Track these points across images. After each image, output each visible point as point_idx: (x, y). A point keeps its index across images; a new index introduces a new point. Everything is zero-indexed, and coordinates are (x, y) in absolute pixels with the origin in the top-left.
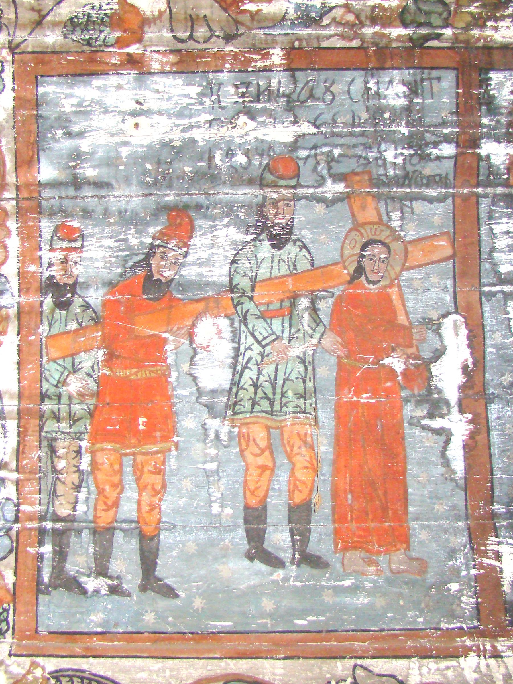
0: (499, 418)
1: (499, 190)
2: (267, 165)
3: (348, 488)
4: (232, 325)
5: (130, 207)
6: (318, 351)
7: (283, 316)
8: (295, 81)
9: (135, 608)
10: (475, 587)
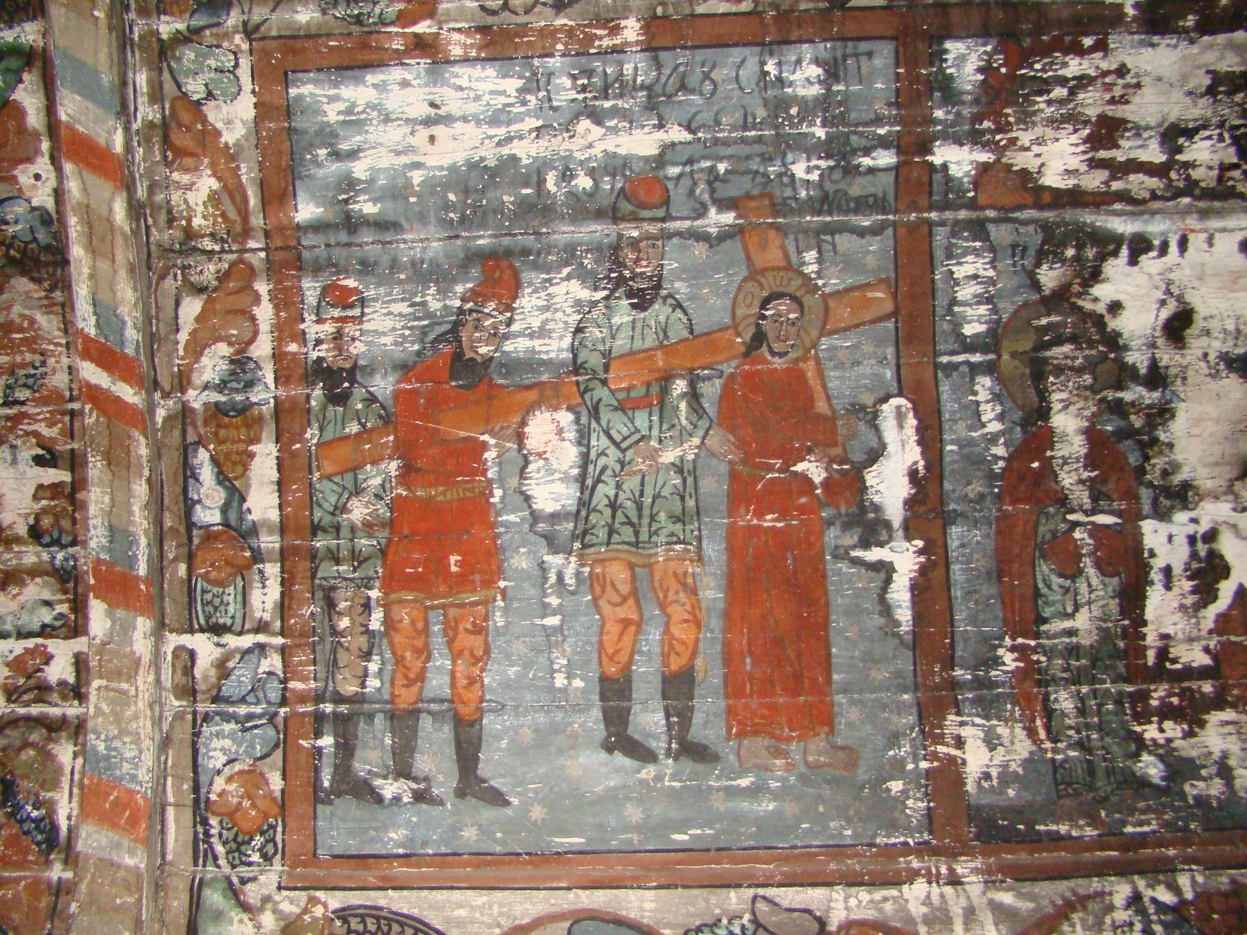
0: (963, 546)
1: (963, 214)
2: (622, 189)
3: (746, 648)
4: (577, 421)
5: (430, 254)
6: (702, 455)
7: (651, 406)
8: (659, 66)
9: (450, 821)
10: (927, 786)
